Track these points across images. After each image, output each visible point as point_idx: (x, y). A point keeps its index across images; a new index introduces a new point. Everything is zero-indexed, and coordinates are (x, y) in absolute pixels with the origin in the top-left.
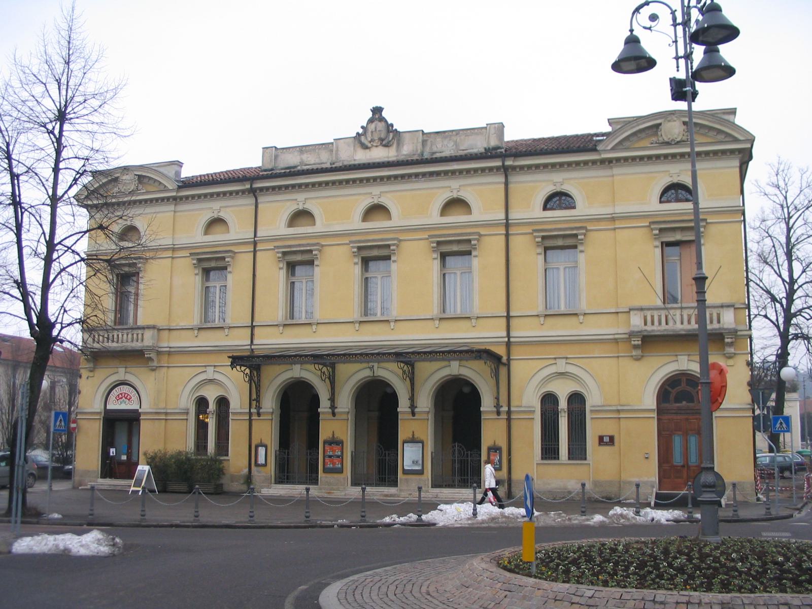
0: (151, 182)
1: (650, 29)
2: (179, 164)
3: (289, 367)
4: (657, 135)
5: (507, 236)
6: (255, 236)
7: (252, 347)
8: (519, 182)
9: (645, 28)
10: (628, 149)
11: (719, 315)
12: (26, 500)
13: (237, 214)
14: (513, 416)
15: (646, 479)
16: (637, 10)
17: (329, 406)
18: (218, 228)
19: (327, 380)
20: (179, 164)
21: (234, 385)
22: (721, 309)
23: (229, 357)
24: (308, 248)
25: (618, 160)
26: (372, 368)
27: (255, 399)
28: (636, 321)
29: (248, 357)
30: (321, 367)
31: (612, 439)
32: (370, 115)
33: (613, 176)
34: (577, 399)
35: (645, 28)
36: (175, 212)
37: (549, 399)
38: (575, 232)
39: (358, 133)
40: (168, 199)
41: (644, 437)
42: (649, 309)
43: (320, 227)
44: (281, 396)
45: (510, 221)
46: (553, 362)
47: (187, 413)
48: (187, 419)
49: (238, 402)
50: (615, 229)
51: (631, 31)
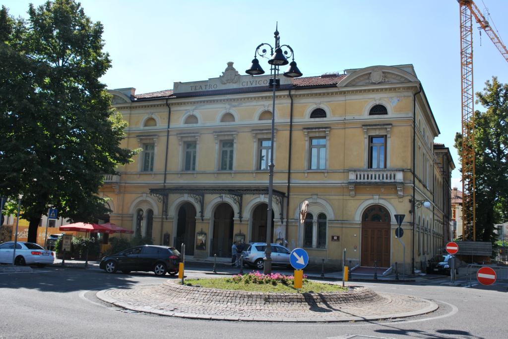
0: (119, 98)
1: (262, 56)
2: (134, 89)
3: (257, 196)
4: (369, 79)
5: (168, 136)
6: (169, 128)
7: (165, 184)
8: (300, 103)
9: (261, 55)
10: (353, 86)
11: (395, 176)
12: (135, 276)
13: (160, 116)
14: (289, 224)
15: (354, 259)
16: (258, 48)
17: (200, 216)
18: (152, 122)
19: (279, 204)
20: (134, 89)
21: (154, 204)
22: (396, 172)
23: (150, 189)
24: (193, 135)
25: (348, 92)
26: (221, 197)
27: (165, 211)
28: (352, 177)
29: (161, 189)
30: (233, 196)
31: (338, 237)
32: (226, 66)
33: (346, 100)
34: (322, 216)
35: (261, 55)
36: (130, 114)
37: (309, 216)
38: (324, 130)
39: (220, 76)
40: (127, 108)
41: (355, 236)
42: (393, 171)
43: (238, 122)
44: (179, 208)
45: (293, 123)
46: (311, 196)
47: (132, 217)
48: (132, 220)
49: (157, 211)
50: (345, 128)
51: (255, 57)
